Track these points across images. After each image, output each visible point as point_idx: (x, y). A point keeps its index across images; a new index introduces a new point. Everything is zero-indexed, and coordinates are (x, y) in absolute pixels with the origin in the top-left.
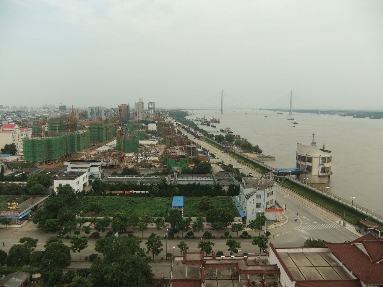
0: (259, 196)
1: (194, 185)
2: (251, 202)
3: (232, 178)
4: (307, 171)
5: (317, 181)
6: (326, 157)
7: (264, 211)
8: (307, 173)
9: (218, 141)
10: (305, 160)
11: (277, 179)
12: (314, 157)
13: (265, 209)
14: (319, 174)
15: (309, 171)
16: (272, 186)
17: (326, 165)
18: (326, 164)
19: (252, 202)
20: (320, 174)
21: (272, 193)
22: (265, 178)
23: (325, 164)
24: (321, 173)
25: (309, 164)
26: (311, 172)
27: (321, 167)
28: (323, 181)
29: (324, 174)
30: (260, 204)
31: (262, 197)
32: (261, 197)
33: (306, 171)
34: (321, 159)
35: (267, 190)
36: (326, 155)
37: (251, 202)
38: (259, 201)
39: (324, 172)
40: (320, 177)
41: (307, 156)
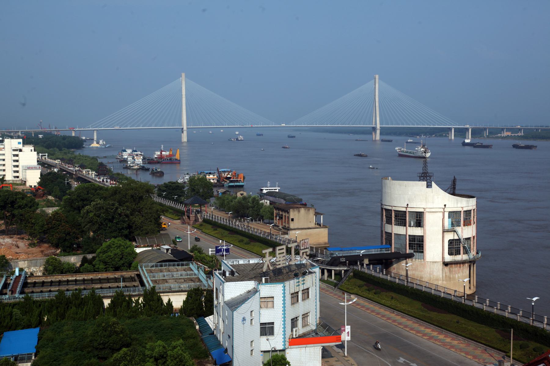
0: (268, 301)
1: (77, 295)
2: (244, 319)
3: (195, 275)
4: (412, 251)
5: (441, 276)
6: (460, 209)
7: (285, 345)
8: (410, 256)
9: (165, 197)
10: (405, 220)
11: (328, 277)
12: (427, 210)
13: (287, 340)
14: (443, 258)
15: (417, 252)
16: (304, 274)
17: (462, 232)
18: (462, 229)
19: (248, 319)
20: (448, 258)
21: (306, 292)
22: (284, 251)
23: (459, 229)
24: (450, 254)
25: (416, 231)
26: (423, 252)
27: (450, 236)
28: (457, 276)
29: (458, 258)
30: (273, 323)
31: (278, 302)
32: (275, 303)
33: (408, 251)
34: (447, 215)
35: (292, 285)
36: (459, 205)
37: (244, 319)
38: (266, 316)
39: (458, 253)
40: (446, 264)
41: (409, 210)
